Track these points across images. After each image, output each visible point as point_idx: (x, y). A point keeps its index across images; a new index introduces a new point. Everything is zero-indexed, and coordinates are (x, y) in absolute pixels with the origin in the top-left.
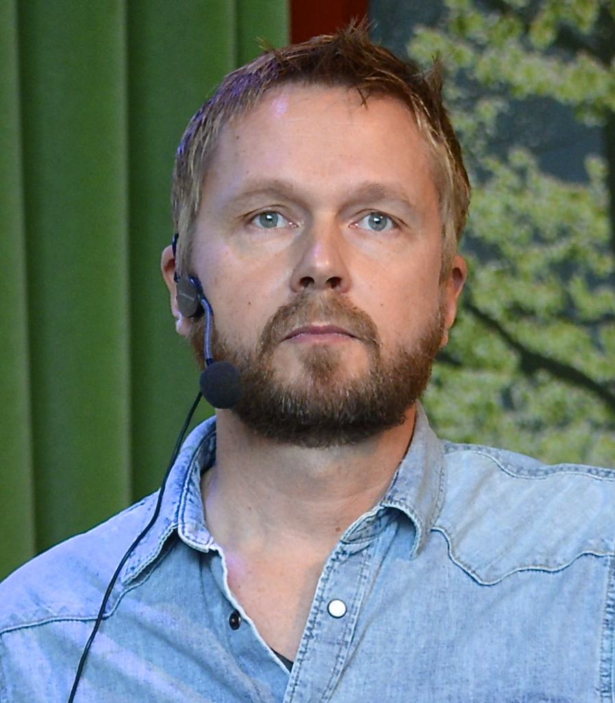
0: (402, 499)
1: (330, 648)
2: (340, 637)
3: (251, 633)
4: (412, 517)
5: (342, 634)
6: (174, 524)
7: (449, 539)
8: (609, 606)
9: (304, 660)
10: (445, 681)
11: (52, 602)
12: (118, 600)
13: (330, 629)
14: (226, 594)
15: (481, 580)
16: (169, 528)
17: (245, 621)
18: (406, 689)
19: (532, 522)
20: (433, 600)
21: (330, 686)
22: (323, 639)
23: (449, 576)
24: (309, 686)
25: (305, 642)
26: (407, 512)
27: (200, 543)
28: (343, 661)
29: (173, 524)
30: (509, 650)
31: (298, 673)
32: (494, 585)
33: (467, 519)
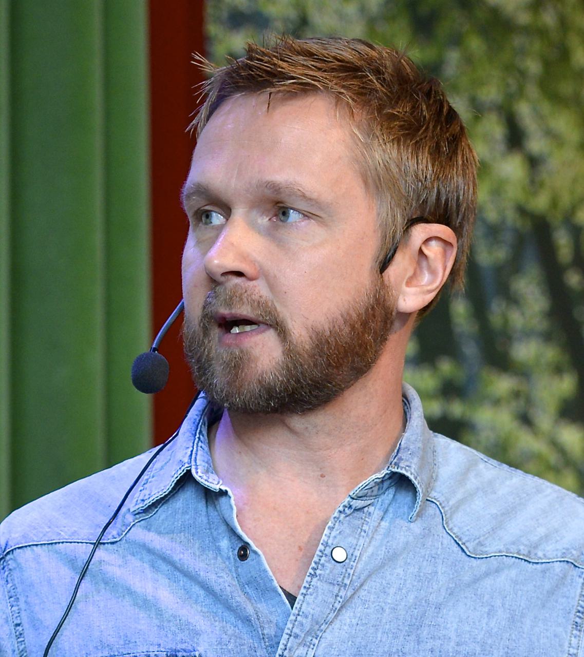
0: (408, 466)
1: (331, 587)
2: (340, 580)
3: (259, 563)
4: (416, 482)
5: (342, 576)
6: (188, 466)
7: (442, 511)
8: (579, 612)
9: (307, 594)
10: (430, 636)
11: (65, 527)
12: (129, 528)
13: (331, 572)
14: (235, 528)
15: (469, 552)
16: (183, 468)
17: (255, 552)
18: (396, 637)
19: (516, 513)
20: (425, 563)
21: (327, 621)
22: (325, 579)
23: (442, 544)
24: (310, 617)
25: (308, 579)
26: (412, 477)
27: (211, 483)
28: (341, 600)
29: (187, 465)
30: (489, 619)
31: (301, 605)
32: (479, 558)
33: (459, 496)
